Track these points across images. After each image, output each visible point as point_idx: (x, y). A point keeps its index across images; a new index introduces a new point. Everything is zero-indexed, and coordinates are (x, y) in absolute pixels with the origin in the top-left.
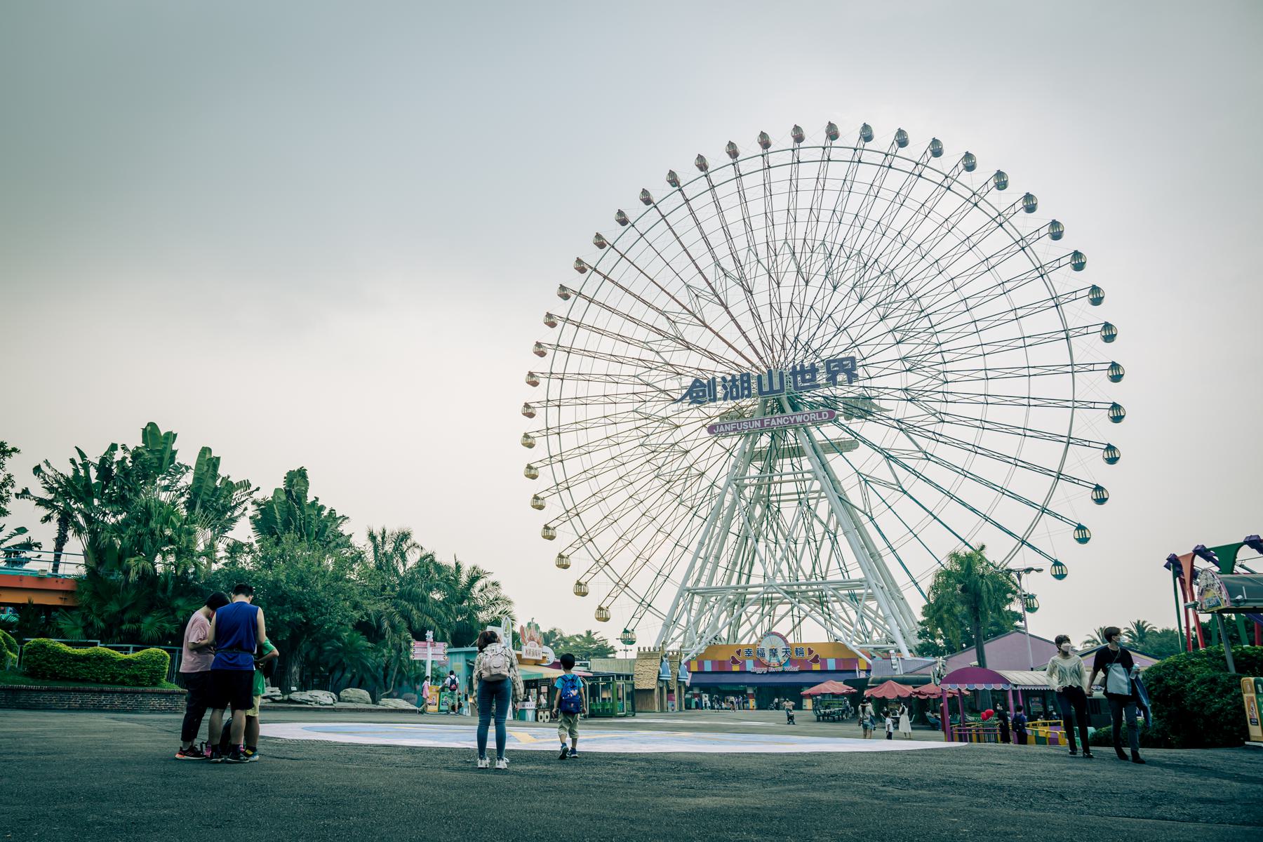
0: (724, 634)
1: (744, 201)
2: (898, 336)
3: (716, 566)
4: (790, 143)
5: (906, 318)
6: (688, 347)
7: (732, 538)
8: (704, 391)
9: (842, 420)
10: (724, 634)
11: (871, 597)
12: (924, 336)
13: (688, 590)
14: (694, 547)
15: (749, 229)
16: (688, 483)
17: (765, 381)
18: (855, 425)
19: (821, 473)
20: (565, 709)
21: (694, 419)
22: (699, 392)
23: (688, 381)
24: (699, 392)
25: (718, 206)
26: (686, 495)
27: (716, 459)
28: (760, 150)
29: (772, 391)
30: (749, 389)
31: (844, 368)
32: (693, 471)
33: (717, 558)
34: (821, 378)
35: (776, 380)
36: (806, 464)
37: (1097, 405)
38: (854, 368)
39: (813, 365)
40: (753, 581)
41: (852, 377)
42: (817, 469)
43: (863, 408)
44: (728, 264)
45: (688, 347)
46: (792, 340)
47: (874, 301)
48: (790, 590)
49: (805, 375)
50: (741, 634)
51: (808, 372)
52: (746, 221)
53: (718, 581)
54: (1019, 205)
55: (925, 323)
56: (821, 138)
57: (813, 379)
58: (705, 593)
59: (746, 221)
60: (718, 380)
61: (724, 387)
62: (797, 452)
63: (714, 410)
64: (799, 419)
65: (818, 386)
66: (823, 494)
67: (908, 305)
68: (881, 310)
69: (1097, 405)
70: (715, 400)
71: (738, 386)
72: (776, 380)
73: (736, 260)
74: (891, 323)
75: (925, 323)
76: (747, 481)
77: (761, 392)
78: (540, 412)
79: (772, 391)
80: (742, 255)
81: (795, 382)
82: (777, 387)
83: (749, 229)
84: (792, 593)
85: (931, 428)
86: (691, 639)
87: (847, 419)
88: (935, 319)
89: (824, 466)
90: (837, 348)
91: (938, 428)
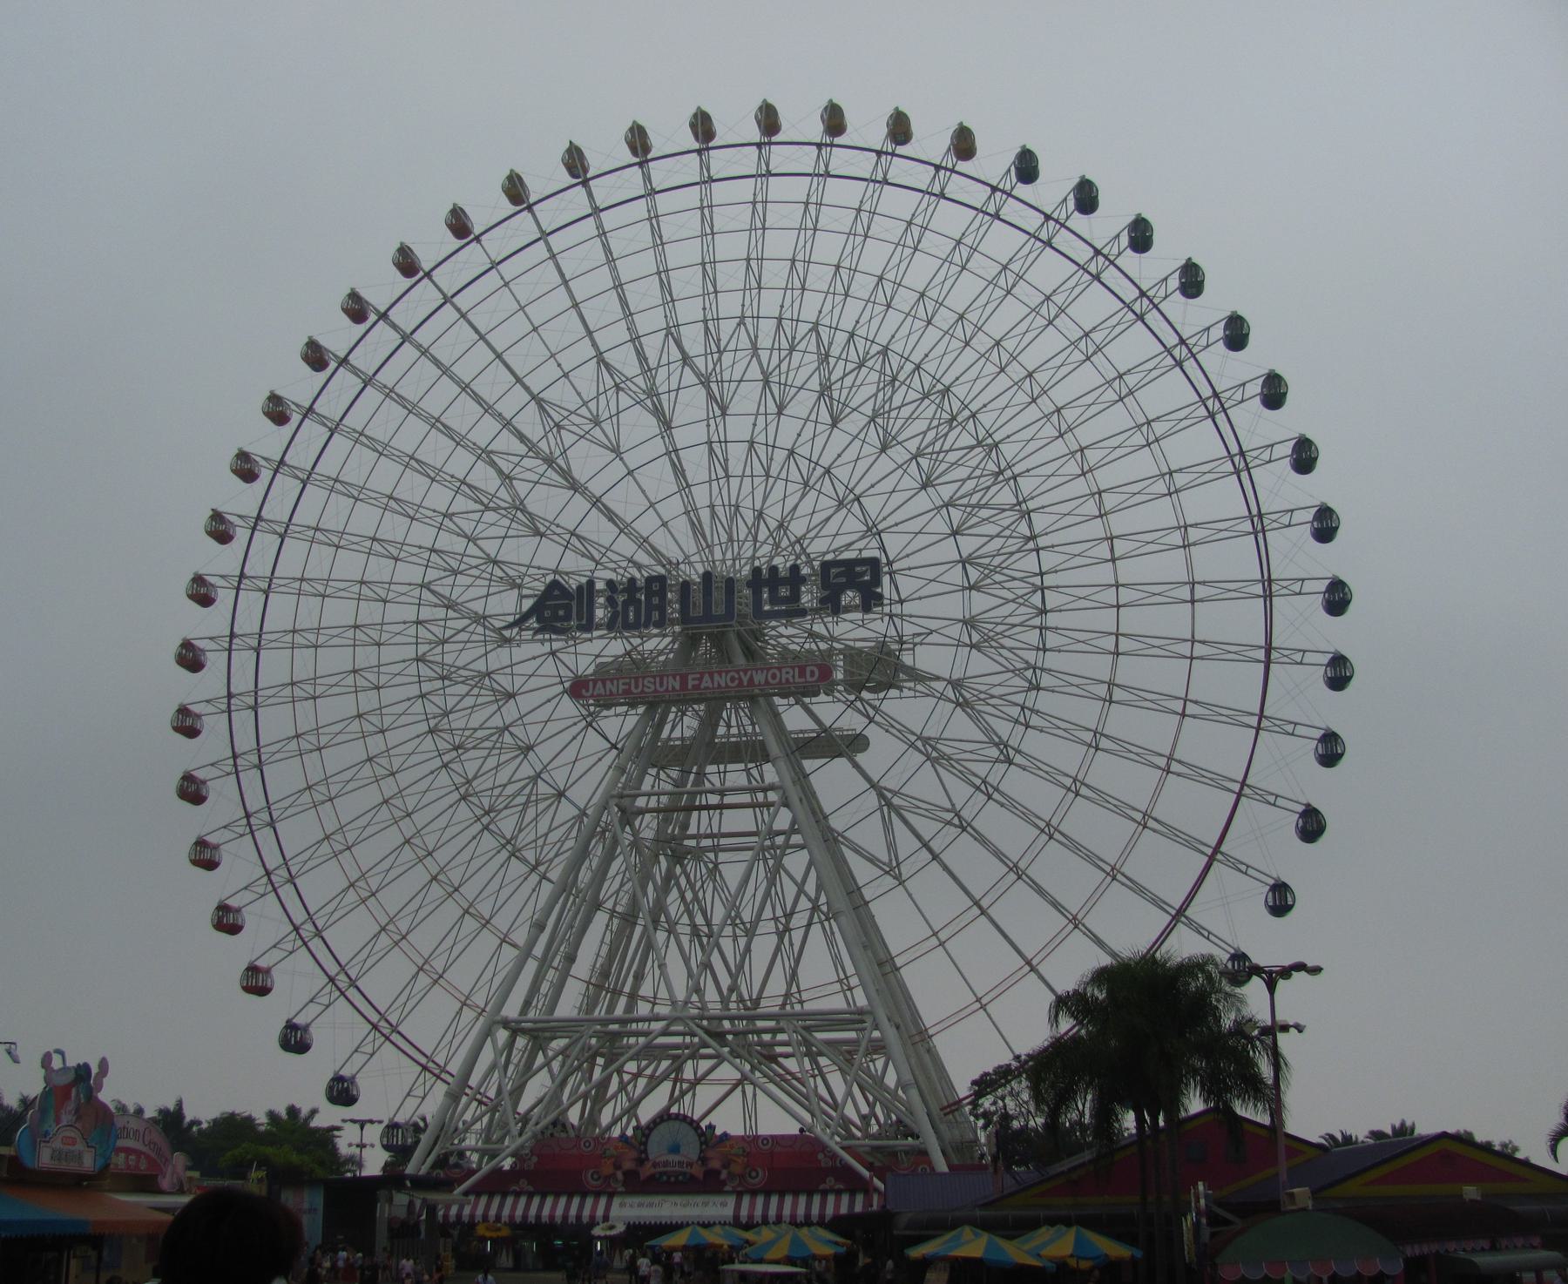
0: (574, 1116)
1: (709, 232)
2: (974, 574)
3: (565, 975)
4: (816, 131)
5: (997, 543)
6: (575, 486)
8: (568, 608)
10: (574, 1116)
11: (878, 1047)
12: (1020, 588)
13: (506, 1024)
14: (520, 937)
15: (712, 289)
16: (531, 813)
17: (697, 597)
19: (794, 795)
21: (541, 667)
24: (558, 609)
25: (656, 232)
26: (526, 837)
27: (583, 756)
28: (755, 134)
29: (708, 617)
31: (856, 581)
32: (543, 788)
34: (808, 597)
35: (718, 595)
36: (770, 773)
37: (1250, 871)
38: (877, 581)
39: (795, 569)
40: (643, 1009)
41: (870, 600)
42: (789, 784)
43: (880, 670)
45: (575, 486)
46: (773, 524)
47: (946, 492)
48: (714, 1027)
49: (777, 588)
50: (606, 1117)
51: (784, 581)
52: (707, 266)
53: (568, 1006)
54: (1174, 282)
55: (1029, 563)
56: (877, 135)
57: (796, 596)
58: (539, 1035)
59: (707, 266)
60: (600, 585)
61: (611, 601)
62: (753, 752)
63: (597, 649)
64: (759, 678)
65: (803, 613)
66: (796, 839)
67: (1008, 518)
68: (956, 515)
70: (589, 626)
71: (639, 601)
72: (718, 595)
74: (968, 545)
75: (1029, 563)
76: (641, 802)
77: (685, 619)
78: (215, 661)
79: (708, 617)
80: (652, 346)
81: (758, 602)
82: (719, 610)
83: (712, 289)
84: (719, 1036)
86: (504, 1125)
88: (1049, 560)
89: (802, 778)
90: (840, 537)
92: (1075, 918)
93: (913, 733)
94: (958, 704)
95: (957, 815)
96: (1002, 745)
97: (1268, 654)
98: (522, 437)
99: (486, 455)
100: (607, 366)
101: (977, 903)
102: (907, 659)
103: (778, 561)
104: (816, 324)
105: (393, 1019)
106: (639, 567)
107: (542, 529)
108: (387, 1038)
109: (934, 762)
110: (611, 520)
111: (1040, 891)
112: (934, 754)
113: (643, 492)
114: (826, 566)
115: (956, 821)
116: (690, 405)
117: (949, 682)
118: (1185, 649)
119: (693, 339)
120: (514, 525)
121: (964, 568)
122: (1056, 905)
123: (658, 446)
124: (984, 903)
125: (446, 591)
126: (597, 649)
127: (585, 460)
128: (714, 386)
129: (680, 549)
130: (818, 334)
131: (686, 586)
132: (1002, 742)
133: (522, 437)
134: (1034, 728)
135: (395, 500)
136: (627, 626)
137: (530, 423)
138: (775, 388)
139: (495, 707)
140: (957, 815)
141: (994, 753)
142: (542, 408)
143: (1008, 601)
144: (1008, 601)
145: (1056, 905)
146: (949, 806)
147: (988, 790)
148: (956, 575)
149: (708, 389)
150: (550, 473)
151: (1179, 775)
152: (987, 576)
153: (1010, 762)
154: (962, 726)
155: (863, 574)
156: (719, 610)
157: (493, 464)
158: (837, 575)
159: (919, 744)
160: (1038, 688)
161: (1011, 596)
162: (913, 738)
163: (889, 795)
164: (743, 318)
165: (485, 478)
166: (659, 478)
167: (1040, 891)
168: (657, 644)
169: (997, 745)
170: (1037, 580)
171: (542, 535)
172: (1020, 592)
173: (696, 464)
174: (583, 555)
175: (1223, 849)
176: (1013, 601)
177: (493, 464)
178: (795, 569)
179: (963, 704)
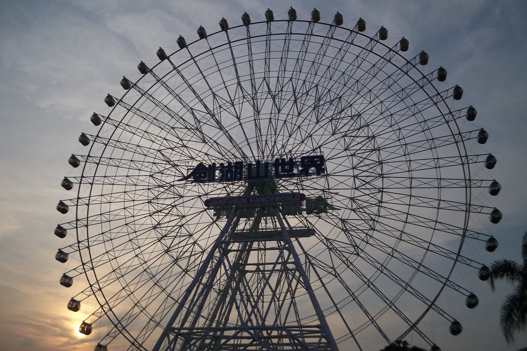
6: (221, 128)
7: (213, 295)
9: (304, 213)
12: (367, 217)
17: (254, 172)
18: (313, 219)
20: (205, 324)
22: (201, 174)
23: (195, 164)
24: (201, 174)
30: (241, 173)
31: (315, 164)
33: (201, 307)
35: (262, 170)
37: (445, 315)
43: (319, 206)
44: (247, 86)
45: (221, 128)
49: (285, 167)
51: (287, 164)
56: (331, 20)
61: (221, 171)
63: (216, 190)
68: (356, 160)
69: (445, 315)
71: (231, 172)
72: (262, 170)
73: (253, 86)
79: (258, 176)
80: (258, 82)
82: (262, 174)
85: (347, 255)
87: (308, 213)
91: (352, 258)
92: (372, 319)
93: (324, 236)
94: (343, 230)
95: (334, 270)
96: (356, 246)
97: (431, 305)
98: (206, 107)
99: (192, 110)
100: (241, 87)
101: (335, 305)
102: (329, 201)
103: (285, 157)
104: (317, 85)
105: (124, 324)
106: (236, 157)
107: (207, 141)
108: (121, 332)
109: (330, 249)
110: (231, 142)
111: (361, 305)
112: (331, 247)
113: (245, 134)
114: (303, 158)
115: (333, 273)
116: (267, 107)
117: (341, 219)
118: (432, 224)
119: (273, 82)
120: (195, 136)
121: (354, 179)
122: (366, 312)
123: (247, 59)
124: (339, 306)
125: (168, 155)
126: (216, 190)
127: (227, 119)
128: (277, 100)
129: (252, 155)
130: (317, 89)
131: (250, 165)
132: (356, 246)
133: (206, 107)
134: (369, 244)
135: (156, 120)
136: (227, 180)
137: (209, 101)
138: (299, 104)
139: (179, 220)
140: (334, 270)
141: (352, 249)
142: (214, 97)
143: (362, 219)
144: (362, 219)
145: (366, 312)
146: (332, 266)
147: (348, 264)
148: (350, 182)
149: (274, 100)
150: (212, 120)
151: (422, 272)
152: (358, 209)
153: (358, 255)
154: (342, 237)
155: (317, 161)
156: (262, 174)
157: (193, 114)
158: (307, 162)
159: (325, 240)
160: (374, 229)
161: (364, 219)
162: (323, 238)
163: (311, 259)
164: (291, 78)
165: (188, 117)
166: (250, 128)
167: (361, 305)
168: (237, 189)
169: (354, 246)
170: (381, 190)
171: (206, 143)
172: (367, 219)
173: (264, 124)
174: (219, 152)
175: (435, 303)
176: (364, 220)
177: (193, 114)
178: (291, 159)
179: (345, 231)
